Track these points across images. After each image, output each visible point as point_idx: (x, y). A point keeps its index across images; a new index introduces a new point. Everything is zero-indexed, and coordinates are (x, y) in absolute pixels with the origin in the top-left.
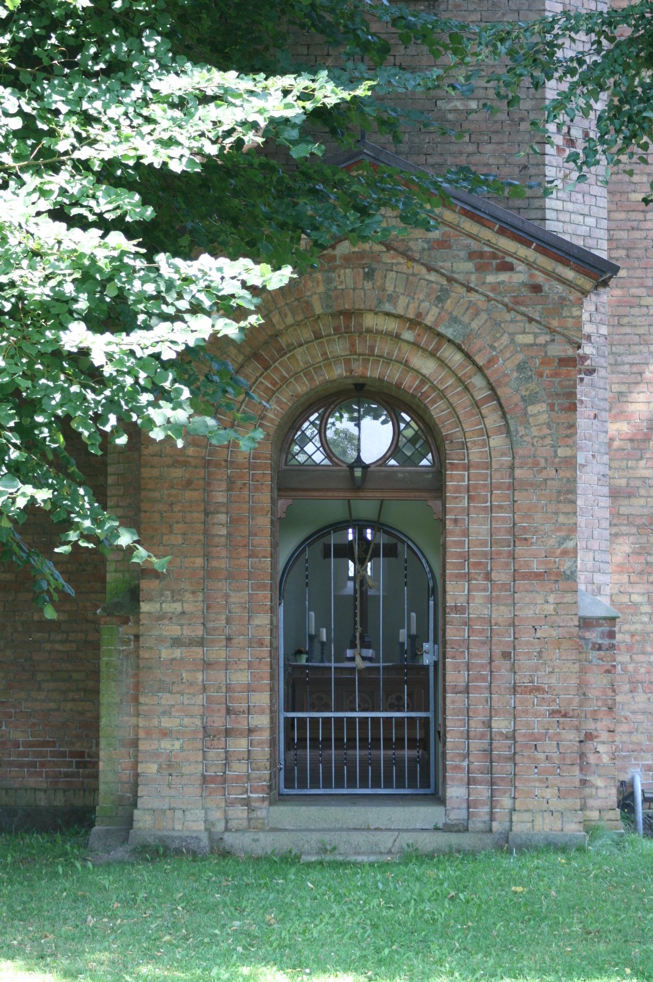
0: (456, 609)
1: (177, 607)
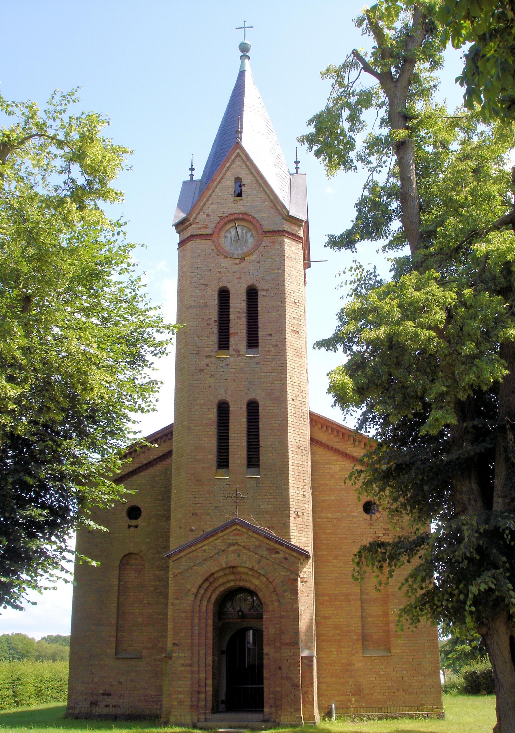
0: (266, 654)
1: (183, 655)
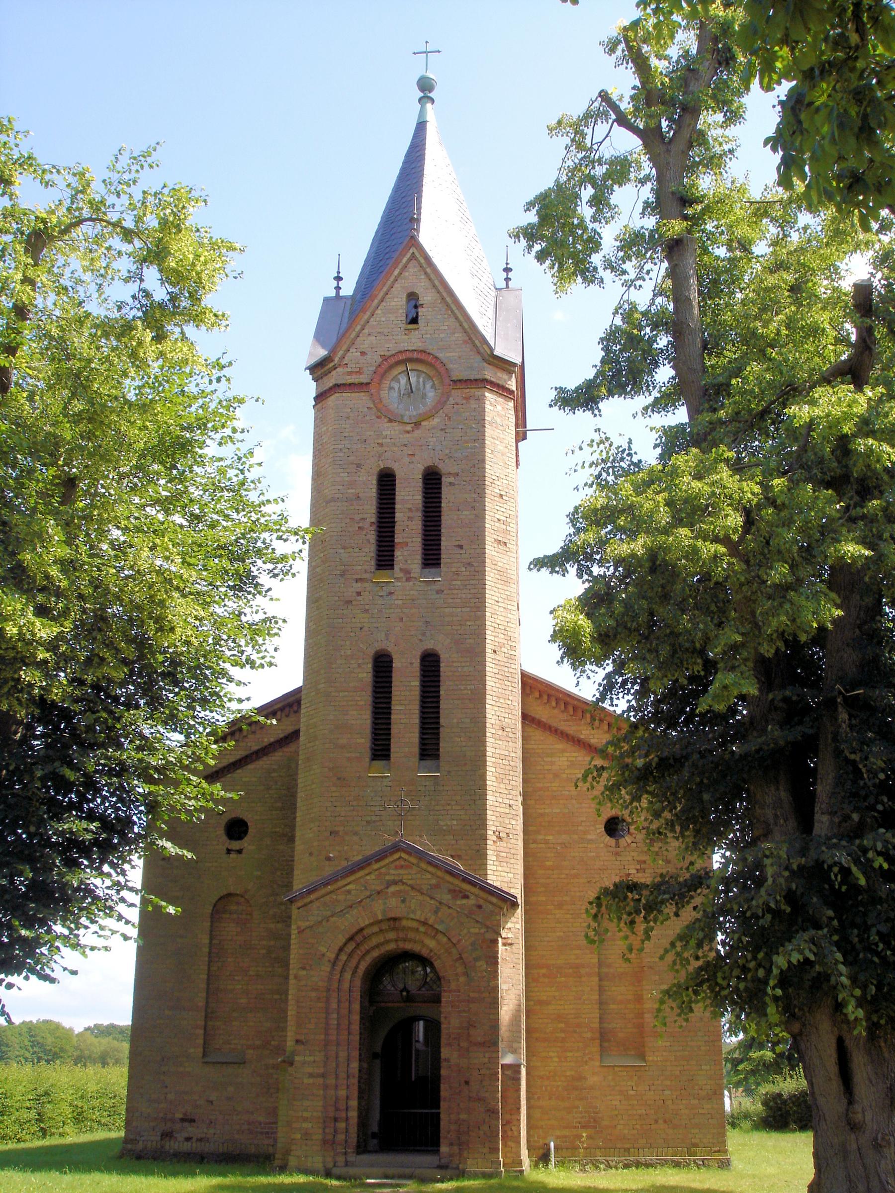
1: (311, 1059)
